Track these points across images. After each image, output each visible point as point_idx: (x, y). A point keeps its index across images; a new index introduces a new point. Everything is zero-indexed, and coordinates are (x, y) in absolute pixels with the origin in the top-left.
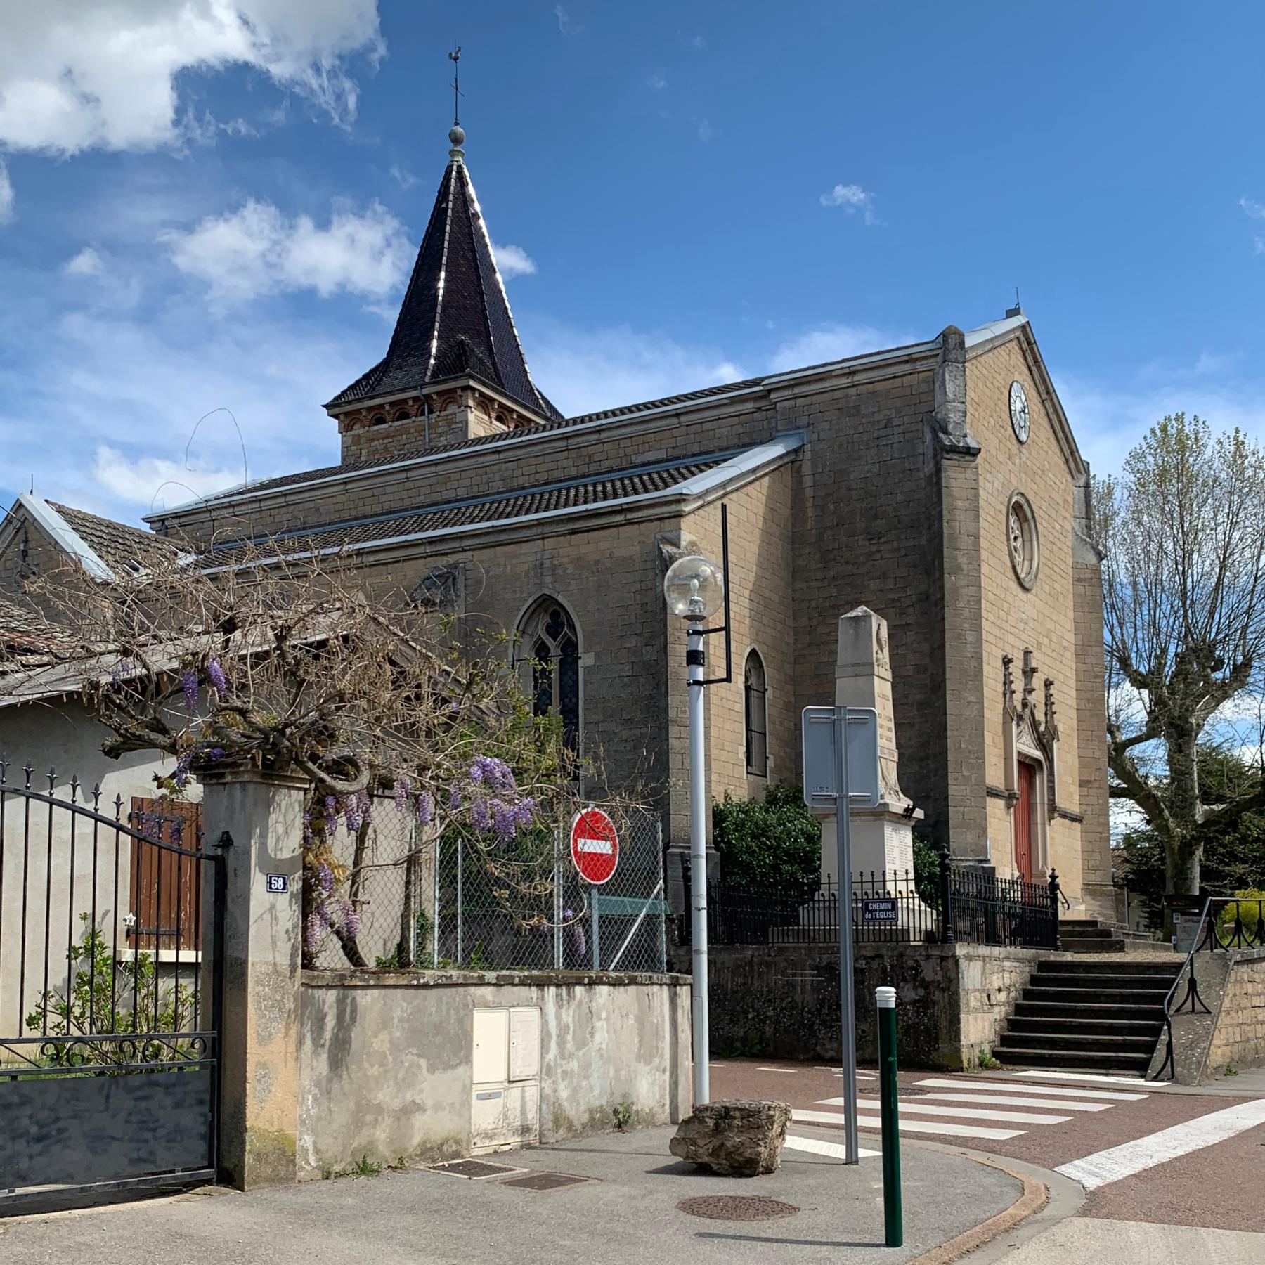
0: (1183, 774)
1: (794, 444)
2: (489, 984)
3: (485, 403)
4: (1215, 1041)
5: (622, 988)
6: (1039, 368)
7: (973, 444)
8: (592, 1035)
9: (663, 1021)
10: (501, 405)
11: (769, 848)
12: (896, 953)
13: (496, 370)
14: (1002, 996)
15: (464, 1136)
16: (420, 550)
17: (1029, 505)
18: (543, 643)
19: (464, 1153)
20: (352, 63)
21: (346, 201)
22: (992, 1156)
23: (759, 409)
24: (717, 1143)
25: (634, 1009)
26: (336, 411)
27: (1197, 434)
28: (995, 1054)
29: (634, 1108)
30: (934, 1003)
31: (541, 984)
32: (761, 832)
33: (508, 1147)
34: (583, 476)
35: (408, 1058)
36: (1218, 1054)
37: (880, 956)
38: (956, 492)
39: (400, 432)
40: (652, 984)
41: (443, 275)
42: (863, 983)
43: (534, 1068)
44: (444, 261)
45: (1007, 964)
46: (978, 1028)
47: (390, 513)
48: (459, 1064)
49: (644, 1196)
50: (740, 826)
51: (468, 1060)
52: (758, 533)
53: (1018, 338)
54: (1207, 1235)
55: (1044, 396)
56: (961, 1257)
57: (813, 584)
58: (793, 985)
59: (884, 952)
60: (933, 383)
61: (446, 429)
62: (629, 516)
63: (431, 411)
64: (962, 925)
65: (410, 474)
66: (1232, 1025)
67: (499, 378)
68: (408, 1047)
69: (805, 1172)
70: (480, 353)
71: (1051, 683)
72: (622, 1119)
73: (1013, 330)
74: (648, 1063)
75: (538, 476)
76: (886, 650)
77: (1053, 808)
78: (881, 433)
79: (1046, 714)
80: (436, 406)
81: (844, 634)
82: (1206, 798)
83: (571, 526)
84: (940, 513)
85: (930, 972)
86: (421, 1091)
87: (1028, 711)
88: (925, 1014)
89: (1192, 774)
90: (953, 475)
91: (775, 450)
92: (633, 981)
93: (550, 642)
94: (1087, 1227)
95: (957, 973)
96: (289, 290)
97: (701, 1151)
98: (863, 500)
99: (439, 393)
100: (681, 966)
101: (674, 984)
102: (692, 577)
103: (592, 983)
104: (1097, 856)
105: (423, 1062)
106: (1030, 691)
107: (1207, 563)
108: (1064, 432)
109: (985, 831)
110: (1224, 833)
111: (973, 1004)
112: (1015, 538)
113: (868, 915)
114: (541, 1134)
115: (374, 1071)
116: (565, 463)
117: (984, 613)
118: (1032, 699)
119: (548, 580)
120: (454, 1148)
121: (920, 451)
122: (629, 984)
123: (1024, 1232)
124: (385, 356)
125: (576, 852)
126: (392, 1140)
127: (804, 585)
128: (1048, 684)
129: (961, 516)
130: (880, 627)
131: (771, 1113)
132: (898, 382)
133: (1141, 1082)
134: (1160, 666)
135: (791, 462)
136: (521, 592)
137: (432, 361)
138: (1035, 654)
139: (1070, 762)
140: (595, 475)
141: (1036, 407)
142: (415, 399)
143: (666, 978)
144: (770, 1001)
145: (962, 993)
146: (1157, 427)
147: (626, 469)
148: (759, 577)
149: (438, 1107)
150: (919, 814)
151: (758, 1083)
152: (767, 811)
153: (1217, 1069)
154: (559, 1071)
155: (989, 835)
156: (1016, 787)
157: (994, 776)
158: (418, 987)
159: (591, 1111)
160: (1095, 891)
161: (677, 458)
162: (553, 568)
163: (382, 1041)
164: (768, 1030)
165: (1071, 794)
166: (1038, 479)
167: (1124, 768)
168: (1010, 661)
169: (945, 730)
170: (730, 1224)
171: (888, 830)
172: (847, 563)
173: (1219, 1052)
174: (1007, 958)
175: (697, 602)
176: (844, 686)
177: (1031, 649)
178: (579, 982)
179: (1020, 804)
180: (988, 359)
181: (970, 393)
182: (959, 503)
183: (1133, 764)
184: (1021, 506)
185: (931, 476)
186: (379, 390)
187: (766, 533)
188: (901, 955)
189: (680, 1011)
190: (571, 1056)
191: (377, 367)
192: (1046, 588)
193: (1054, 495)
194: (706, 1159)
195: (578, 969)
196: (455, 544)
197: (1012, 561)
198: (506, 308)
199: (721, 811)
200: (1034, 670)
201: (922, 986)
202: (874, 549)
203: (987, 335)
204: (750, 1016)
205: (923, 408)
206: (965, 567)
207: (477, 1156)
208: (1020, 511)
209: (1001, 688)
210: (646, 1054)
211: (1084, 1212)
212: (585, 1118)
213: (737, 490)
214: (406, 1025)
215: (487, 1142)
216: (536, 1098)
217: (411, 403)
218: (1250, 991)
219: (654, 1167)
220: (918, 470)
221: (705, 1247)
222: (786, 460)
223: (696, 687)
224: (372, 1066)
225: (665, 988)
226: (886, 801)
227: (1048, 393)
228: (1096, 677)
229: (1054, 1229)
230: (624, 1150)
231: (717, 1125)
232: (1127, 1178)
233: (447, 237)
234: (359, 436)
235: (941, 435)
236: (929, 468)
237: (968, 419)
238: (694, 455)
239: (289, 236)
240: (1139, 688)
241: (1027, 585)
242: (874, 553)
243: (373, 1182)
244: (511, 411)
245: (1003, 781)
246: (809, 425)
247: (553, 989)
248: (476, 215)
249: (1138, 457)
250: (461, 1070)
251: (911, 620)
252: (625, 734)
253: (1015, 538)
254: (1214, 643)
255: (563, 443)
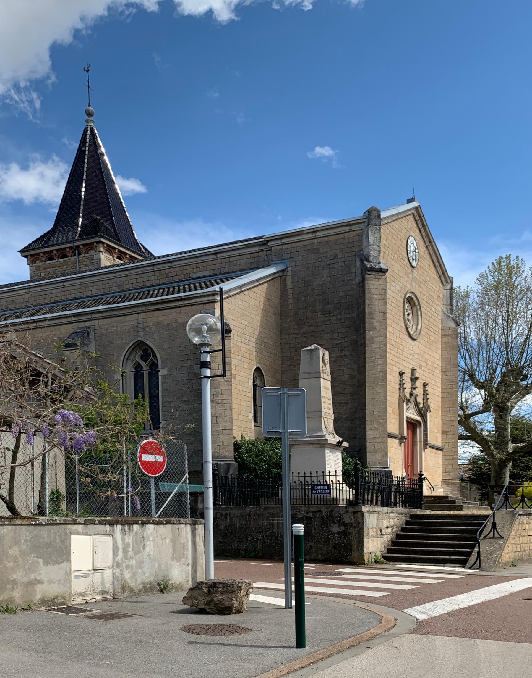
0: (502, 429)
1: (281, 267)
2: (80, 524)
3: (110, 250)
4: (505, 551)
5: (162, 526)
6: (425, 229)
7: (383, 266)
8: (144, 548)
9: (188, 541)
10: (119, 251)
11: (265, 461)
12: (329, 510)
13: (116, 234)
14: (389, 530)
15: (67, 595)
16: (69, 319)
17: (417, 298)
18: (139, 364)
19: (68, 603)
20: (37, 84)
21: (37, 155)
22: (369, 605)
23: (262, 250)
24: (209, 599)
25: (170, 536)
26: (26, 254)
27: (518, 265)
28: (383, 557)
29: (170, 582)
30: (350, 533)
31: (112, 524)
32: (260, 453)
33: (95, 600)
34: (163, 284)
35: (32, 558)
36: (507, 556)
37: (321, 511)
38: (373, 291)
39: (62, 264)
40: (181, 524)
41: (84, 185)
42: (311, 524)
43: (109, 564)
44: (84, 177)
45: (392, 515)
46: (374, 545)
47: (55, 303)
48: (63, 562)
49: (163, 624)
50: (249, 451)
51: (68, 560)
52: (260, 311)
53: (413, 214)
54: (480, 643)
55: (428, 244)
56: (338, 653)
57: (292, 336)
58: (273, 525)
59: (323, 509)
60: (362, 236)
61: (88, 262)
62: (186, 302)
63: (79, 254)
64: (367, 497)
65: (65, 284)
66: (515, 544)
67: (118, 238)
68: (31, 553)
69: (260, 612)
70: (107, 225)
71: (427, 385)
72: (163, 588)
73: (410, 210)
74: (178, 560)
75: (137, 284)
76: (328, 366)
77: (426, 444)
78: (332, 262)
79: (423, 399)
80: (82, 251)
81: (304, 357)
82: (515, 440)
83: (154, 307)
84: (364, 301)
85: (347, 519)
86: (40, 574)
87: (413, 398)
88: (345, 538)
89: (507, 429)
90: (373, 282)
91: (271, 270)
92: (168, 522)
93: (143, 363)
94: (413, 639)
95: (363, 519)
96: (8, 201)
97: (200, 603)
98: (320, 295)
99: (83, 245)
100: (198, 514)
101: (194, 524)
102: (203, 325)
103: (143, 523)
104: (450, 467)
105: (41, 561)
106: (415, 388)
107: (521, 329)
108: (439, 262)
109: (387, 454)
110: (524, 456)
111: (371, 533)
112: (408, 315)
113: (314, 492)
114: (114, 594)
115: (11, 564)
116: (153, 278)
117: (388, 350)
118: (415, 392)
119: (141, 333)
120: (61, 600)
121: (354, 271)
122: (166, 524)
123: (377, 641)
124: (52, 227)
125: (141, 461)
126: (23, 596)
127: (287, 337)
128: (425, 385)
129: (376, 303)
130: (324, 355)
131: (240, 585)
132: (342, 236)
133: (463, 570)
134: (493, 378)
135: (280, 276)
136: (127, 340)
137: (79, 229)
138: (418, 370)
139: (437, 422)
140: (169, 283)
141: (423, 249)
142: (70, 248)
143: (189, 521)
144: (260, 532)
145: (365, 529)
146: (495, 262)
147: (187, 280)
148: (261, 333)
149: (50, 582)
150: (346, 444)
151: (234, 570)
152: (264, 444)
153: (505, 564)
154: (124, 565)
155: (389, 456)
156: (405, 433)
157: (393, 427)
158: (36, 525)
159: (144, 584)
160: (449, 483)
161: (216, 275)
162: (144, 328)
163: (15, 551)
164: (259, 546)
165: (437, 437)
166: (422, 285)
167: (469, 426)
168: (403, 373)
169: (365, 406)
170: (209, 637)
171: (328, 452)
172: (312, 325)
173: (507, 556)
174: (392, 513)
175: (206, 337)
176: (303, 384)
177: (416, 368)
178: (136, 523)
179: (409, 441)
180: (395, 224)
181: (383, 242)
182: (375, 296)
183: (474, 424)
184: (412, 299)
185: (359, 283)
186: (50, 243)
187: (265, 310)
188: (332, 511)
189: (197, 537)
190: (131, 558)
191: (48, 232)
192: (426, 339)
193: (432, 293)
194: (203, 607)
195: (142, 515)
196: (89, 317)
197: (406, 326)
198: (121, 202)
199: (239, 444)
200: (417, 378)
201: (343, 525)
202: (327, 319)
203: (394, 211)
204: (249, 539)
205: (356, 249)
206: (378, 328)
207: (75, 604)
208: (411, 301)
209: (398, 387)
210: (177, 556)
211: (413, 631)
212: (141, 587)
213: (248, 289)
214: (29, 543)
215: (81, 598)
216: (111, 578)
217: (68, 250)
218: (527, 528)
219: (175, 610)
220: (352, 280)
221: (191, 648)
222: (277, 275)
223: (206, 379)
224: (9, 562)
225: (189, 526)
226: (327, 438)
227: (430, 242)
228: (453, 382)
229: (394, 639)
230: (161, 602)
231: (209, 591)
232: (441, 615)
233: (86, 165)
234: (39, 266)
235: (365, 262)
236: (358, 279)
237: (382, 254)
238: (225, 273)
239: (6, 173)
240: (479, 389)
241: (414, 337)
242: (327, 321)
243: (11, 616)
244: (126, 254)
245: (398, 431)
246: (290, 258)
247: (119, 527)
248: (102, 154)
249: (483, 277)
250: (64, 564)
251: (347, 353)
252: (185, 407)
253: (408, 315)
254: (523, 368)
255: (152, 268)
